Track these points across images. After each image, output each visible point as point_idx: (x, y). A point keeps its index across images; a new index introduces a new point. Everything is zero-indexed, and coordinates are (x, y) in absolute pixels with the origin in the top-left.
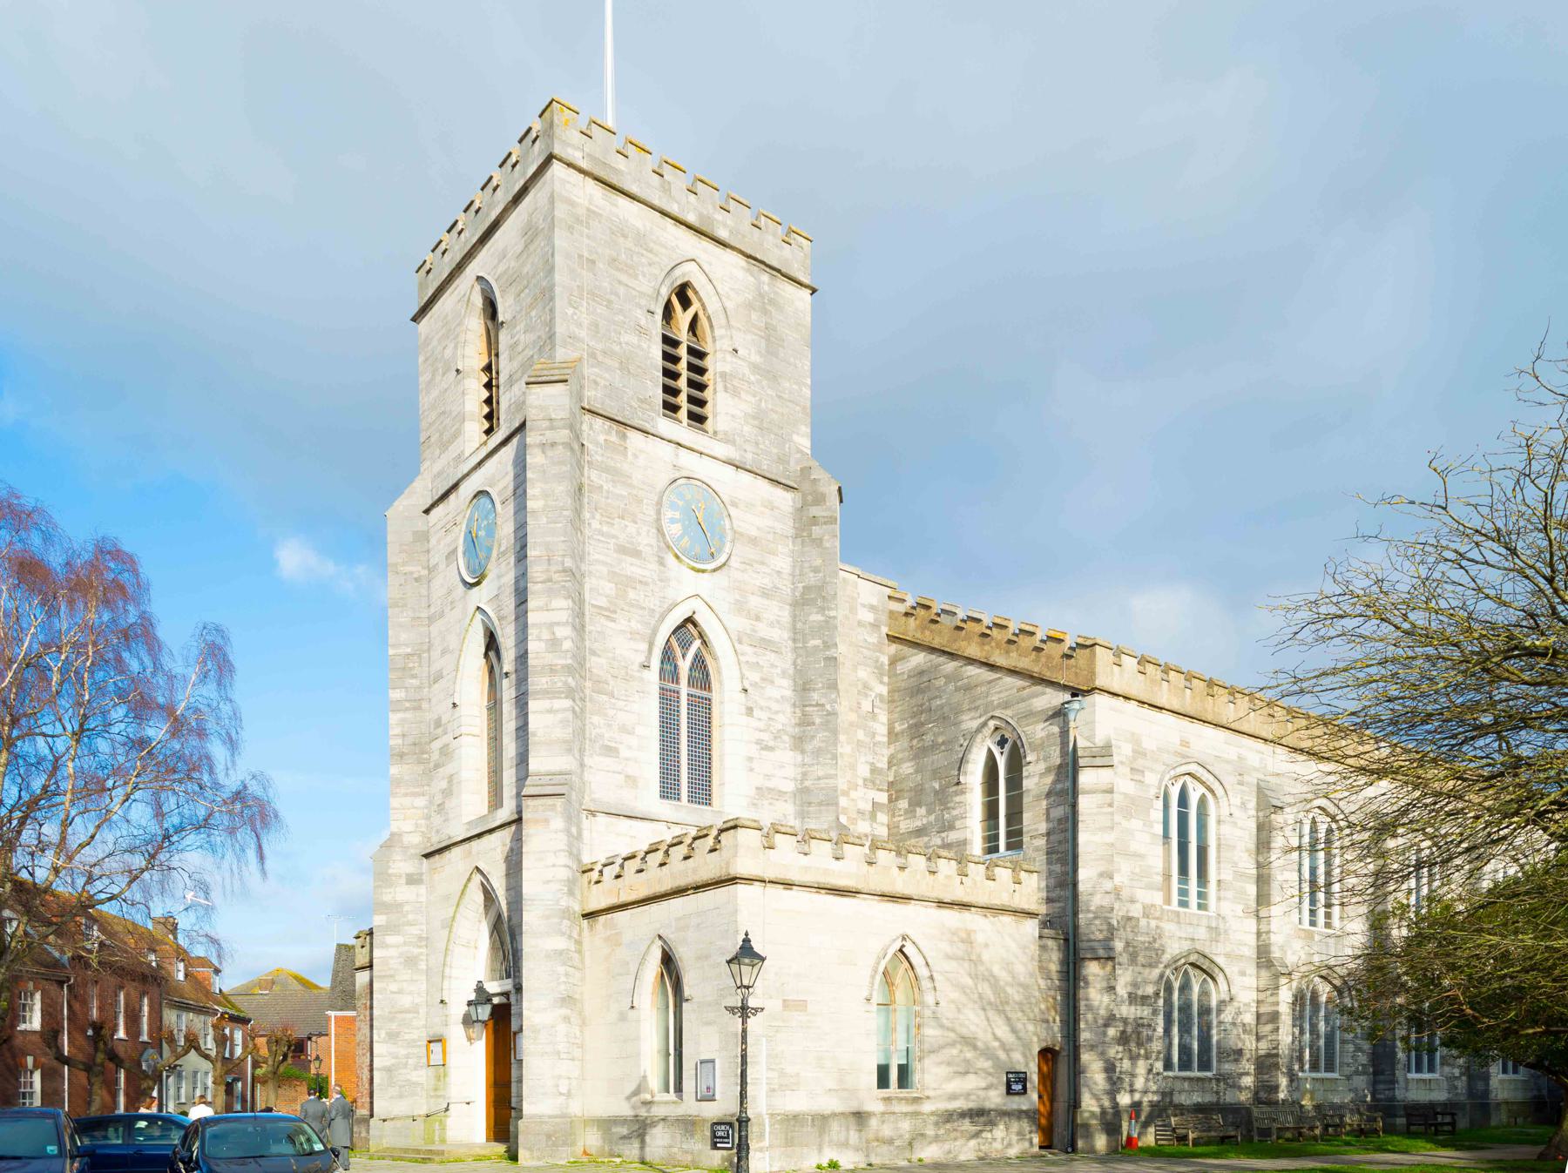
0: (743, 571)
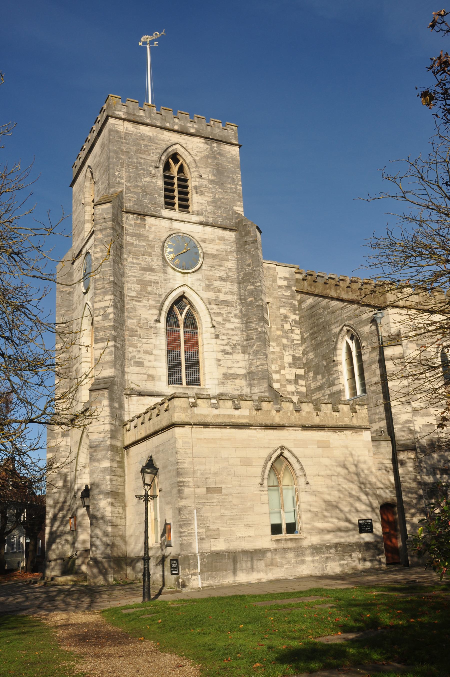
0: (209, 271)
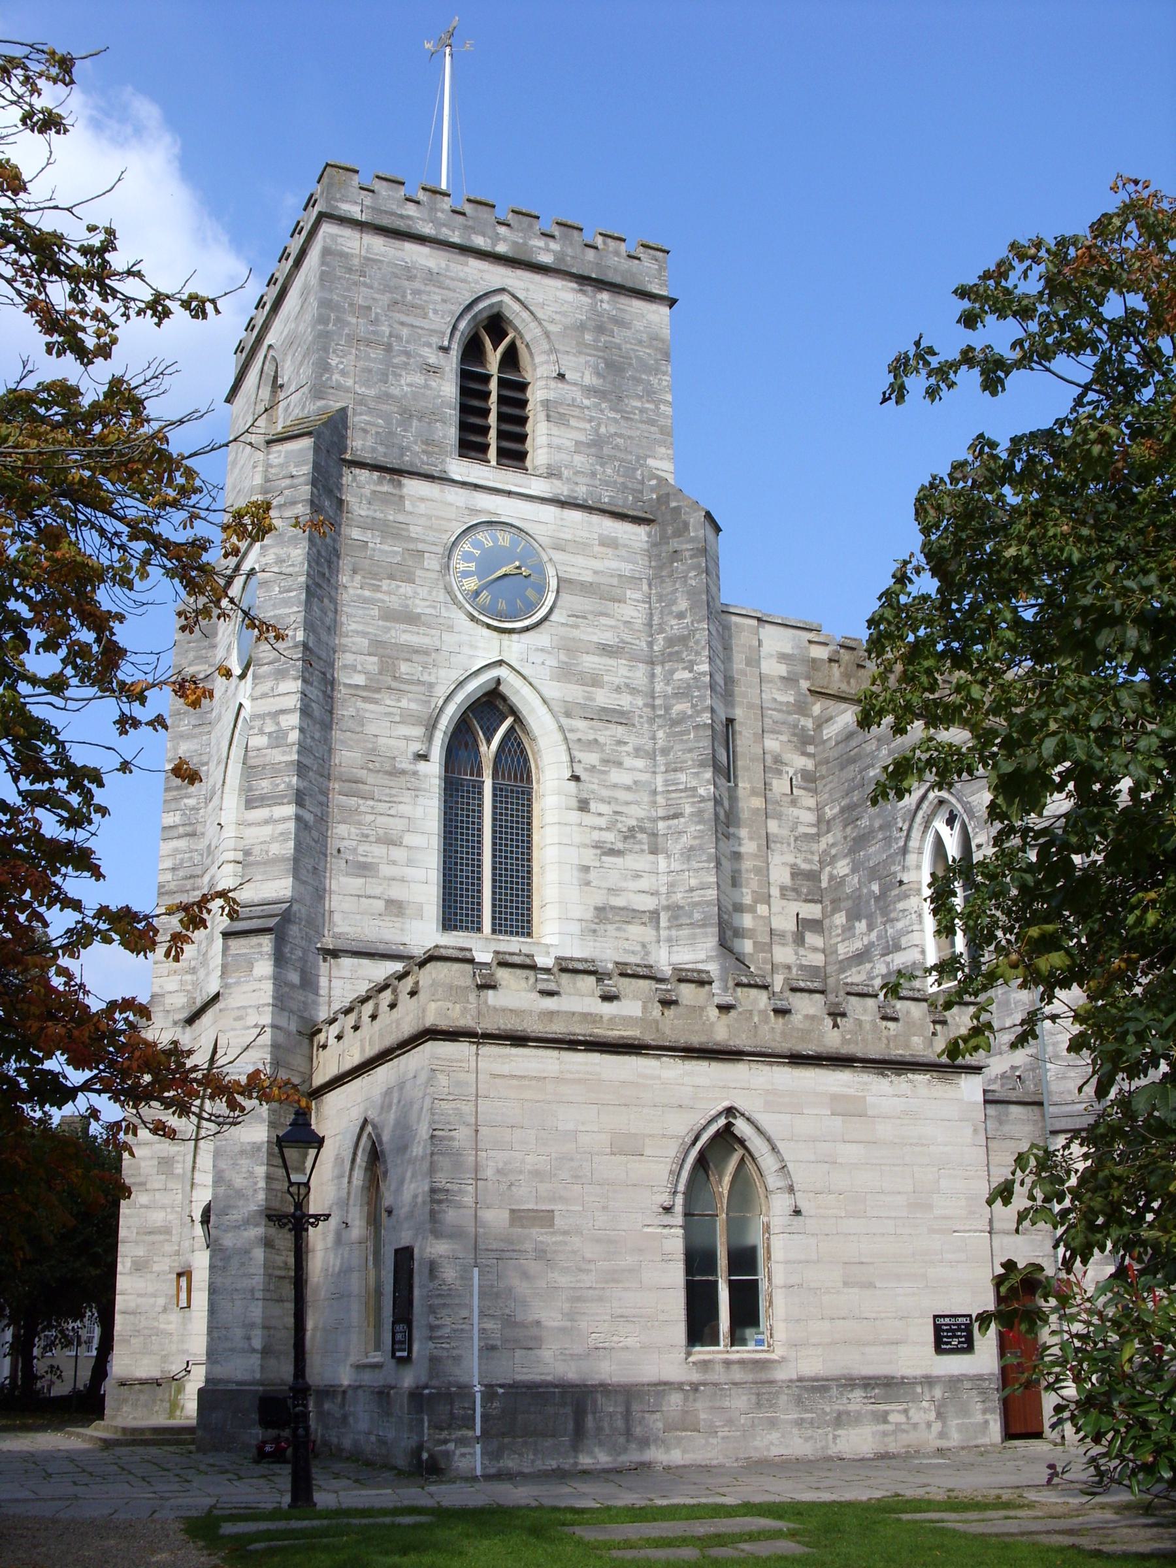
0: (572, 626)
